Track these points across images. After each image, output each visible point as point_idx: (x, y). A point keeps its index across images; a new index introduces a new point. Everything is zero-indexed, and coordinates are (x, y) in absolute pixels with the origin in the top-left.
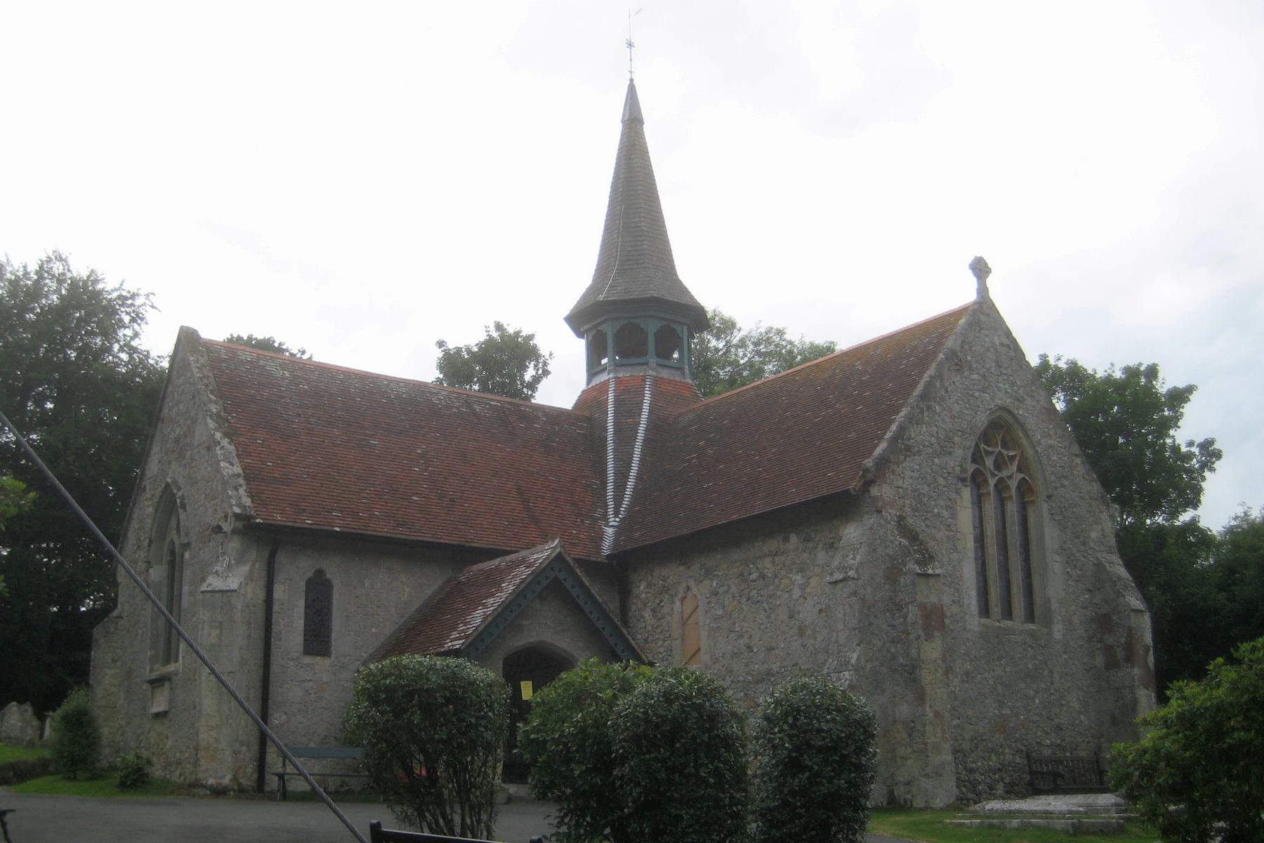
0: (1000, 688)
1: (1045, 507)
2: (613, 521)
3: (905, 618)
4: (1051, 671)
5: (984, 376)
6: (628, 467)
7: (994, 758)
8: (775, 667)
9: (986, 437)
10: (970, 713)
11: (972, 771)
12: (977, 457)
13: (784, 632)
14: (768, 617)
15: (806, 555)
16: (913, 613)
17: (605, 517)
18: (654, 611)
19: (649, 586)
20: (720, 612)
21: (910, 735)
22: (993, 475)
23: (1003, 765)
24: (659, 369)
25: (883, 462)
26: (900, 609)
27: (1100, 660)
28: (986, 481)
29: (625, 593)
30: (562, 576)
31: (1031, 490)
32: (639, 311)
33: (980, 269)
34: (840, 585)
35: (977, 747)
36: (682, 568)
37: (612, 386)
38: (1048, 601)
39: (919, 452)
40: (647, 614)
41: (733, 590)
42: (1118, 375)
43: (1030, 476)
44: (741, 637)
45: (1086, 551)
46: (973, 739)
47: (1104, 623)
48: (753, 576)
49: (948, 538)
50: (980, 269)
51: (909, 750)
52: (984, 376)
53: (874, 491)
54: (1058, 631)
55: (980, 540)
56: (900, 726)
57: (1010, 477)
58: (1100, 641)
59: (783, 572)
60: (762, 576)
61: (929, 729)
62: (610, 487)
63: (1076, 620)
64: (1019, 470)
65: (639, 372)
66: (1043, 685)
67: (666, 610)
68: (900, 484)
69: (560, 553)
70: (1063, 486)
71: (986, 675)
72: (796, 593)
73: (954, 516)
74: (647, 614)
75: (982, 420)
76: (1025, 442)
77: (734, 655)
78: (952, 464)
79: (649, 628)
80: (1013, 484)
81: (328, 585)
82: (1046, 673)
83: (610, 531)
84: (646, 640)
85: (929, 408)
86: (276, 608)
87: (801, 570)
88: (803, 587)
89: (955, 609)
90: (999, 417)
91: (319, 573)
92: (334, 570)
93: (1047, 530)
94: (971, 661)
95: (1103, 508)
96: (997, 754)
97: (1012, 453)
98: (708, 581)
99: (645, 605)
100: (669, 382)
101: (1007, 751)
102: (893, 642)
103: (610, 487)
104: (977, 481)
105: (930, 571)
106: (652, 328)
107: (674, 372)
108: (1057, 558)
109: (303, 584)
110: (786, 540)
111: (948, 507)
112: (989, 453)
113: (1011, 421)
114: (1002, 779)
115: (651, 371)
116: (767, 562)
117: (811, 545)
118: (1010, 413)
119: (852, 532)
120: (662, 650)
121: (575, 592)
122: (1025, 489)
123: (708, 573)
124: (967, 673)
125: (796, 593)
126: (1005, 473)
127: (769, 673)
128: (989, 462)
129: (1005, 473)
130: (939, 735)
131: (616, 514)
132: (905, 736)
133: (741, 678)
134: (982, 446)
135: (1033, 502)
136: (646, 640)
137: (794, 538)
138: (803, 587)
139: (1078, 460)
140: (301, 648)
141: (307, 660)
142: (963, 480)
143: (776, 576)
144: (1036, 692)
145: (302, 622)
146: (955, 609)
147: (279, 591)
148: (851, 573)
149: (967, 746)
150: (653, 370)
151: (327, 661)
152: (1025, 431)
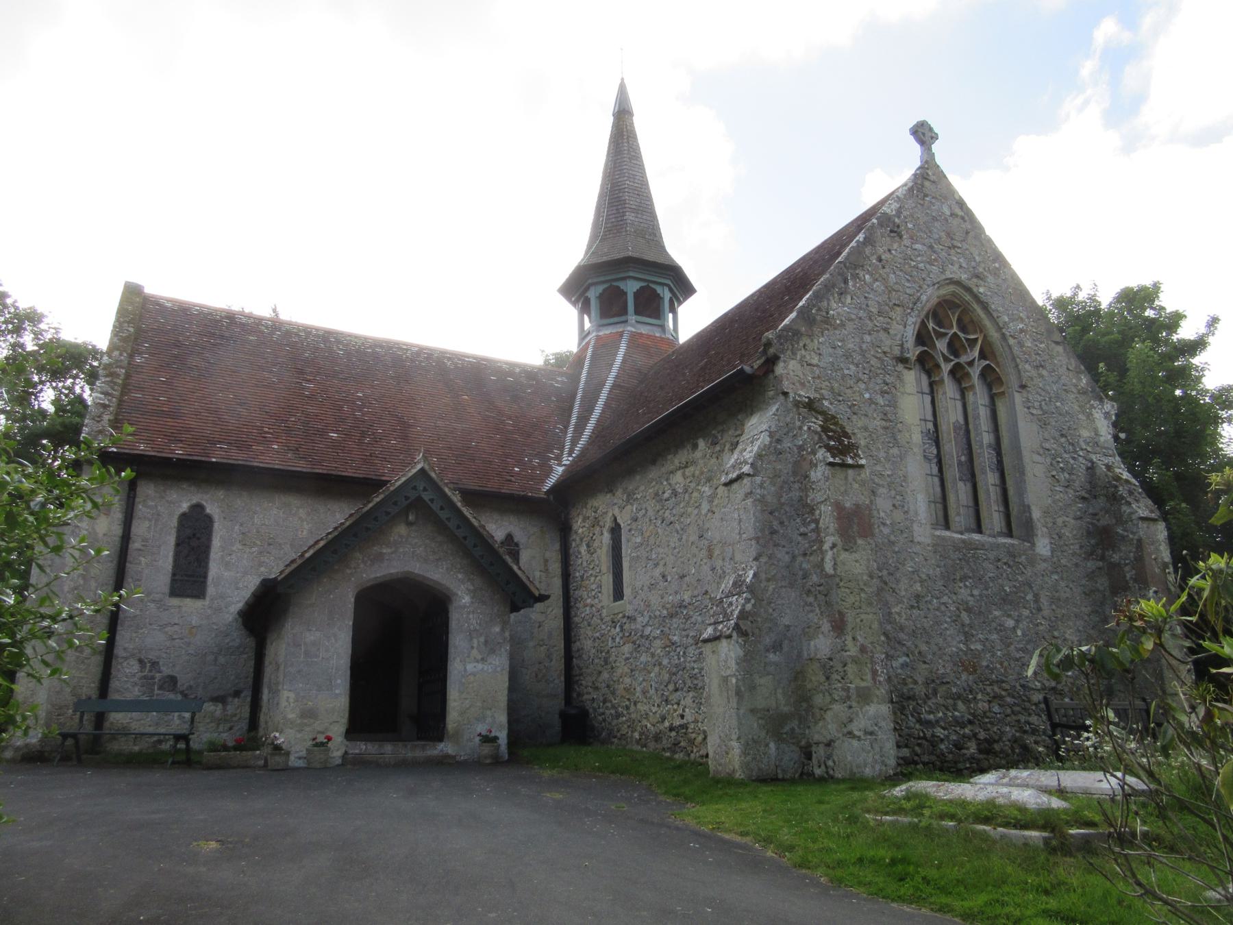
0: (964, 616)
1: (1018, 398)
2: (567, 460)
3: (817, 522)
4: (1036, 596)
5: (931, 247)
6: (587, 419)
7: (960, 705)
8: (686, 597)
9: (939, 313)
10: (924, 648)
11: (928, 724)
12: (922, 337)
13: (694, 556)
14: (680, 540)
15: (714, 460)
16: (826, 515)
17: (559, 459)
18: (588, 546)
19: (585, 519)
20: (639, 540)
21: (828, 678)
22: (947, 360)
23: (974, 715)
24: (639, 326)
25: (792, 334)
26: (812, 511)
27: (1103, 583)
28: (938, 366)
29: (564, 531)
30: (426, 497)
31: (999, 380)
32: (627, 274)
33: (923, 134)
34: (735, 486)
35: (935, 693)
36: (609, 496)
37: (626, 337)
38: (1027, 509)
39: (843, 325)
40: (583, 549)
41: (651, 513)
42: (1106, 300)
43: (998, 364)
44: (656, 565)
45: (1075, 452)
46: (927, 684)
47: (1103, 538)
48: (666, 495)
49: (886, 428)
50: (923, 134)
51: (828, 699)
52: (931, 247)
53: (780, 369)
54: (1043, 546)
55: (935, 437)
56: (816, 666)
57: (971, 363)
58: (1103, 558)
59: (693, 485)
60: (675, 493)
61: (851, 669)
62: (571, 429)
63: (1067, 532)
64: (983, 355)
65: (619, 328)
66: (1026, 613)
67: (596, 544)
68: (815, 361)
69: (422, 470)
70: (1041, 376)
71: (945, 599)
72: (705, 507)
73: (893, 404)
74: (583, 549)
75: (929, 297)
76: (987, 323)
77: (652, 586)
78: (888, 342)
79: (585, 564)
80: (975, 373)
81: (209, 520)
82: (1029, 597)
83: (560, 469)
84: (582, 577)
85: (855, 276)
86: (135, 545)
87: (709, 480)
88: (711, 499)
89: (898, 516)
90: (954, 294)
91: (198, 508)
92: (214, 503)
93: (1021, 424)
94: (922, 581)
95: (1095, 403)
96: (966, 701)
97: (972, 337)
98: (629, 507)
99: (581, 540)
100: (649, 337)
101: (979, 696)
102: (805, 555)
103: (571, 429)
104: (926, 363)
105: (850, 461)
106: (631, 287)
107: (655, 328)
108: (1037, 458)
109: (174, 522)
110: (695, 446)
111: (883, 393)
112: (941, 336)
113: (968, 297)
114: (975, 735)
115: (635, 325)
116: (678, 478)
117: (718, 448)
118: (968, 290)
119: (758, 429)
120: (594, 587)
121: (443, 515)
122: (990, 377)
123: (630, 498)
124: (918, 597)
125: (705, 507)
126: (963, 359)
127: (682, 606)
128: (941, 345)
129: (963, 359)
130: (869, 677)
131: (570, 454)
132: (823, 679)
133: (658, 613)
134: (931, 325)
135: (1003, 393)
136: (582, 577)
137: (702, 444)
138: (711, 499)
139: (1060, 349)
140: (167, 590)
141: (175, 601)
142: (903, 360)
143: (686, 491)
144: (1017, 621)
145: (171, 559)
146: (898, 516)
147: (140, 528)
148: (746, 469)
149: (920, 690)
150: (632, 326)
151: (199, 604)
152: (985, 306)
